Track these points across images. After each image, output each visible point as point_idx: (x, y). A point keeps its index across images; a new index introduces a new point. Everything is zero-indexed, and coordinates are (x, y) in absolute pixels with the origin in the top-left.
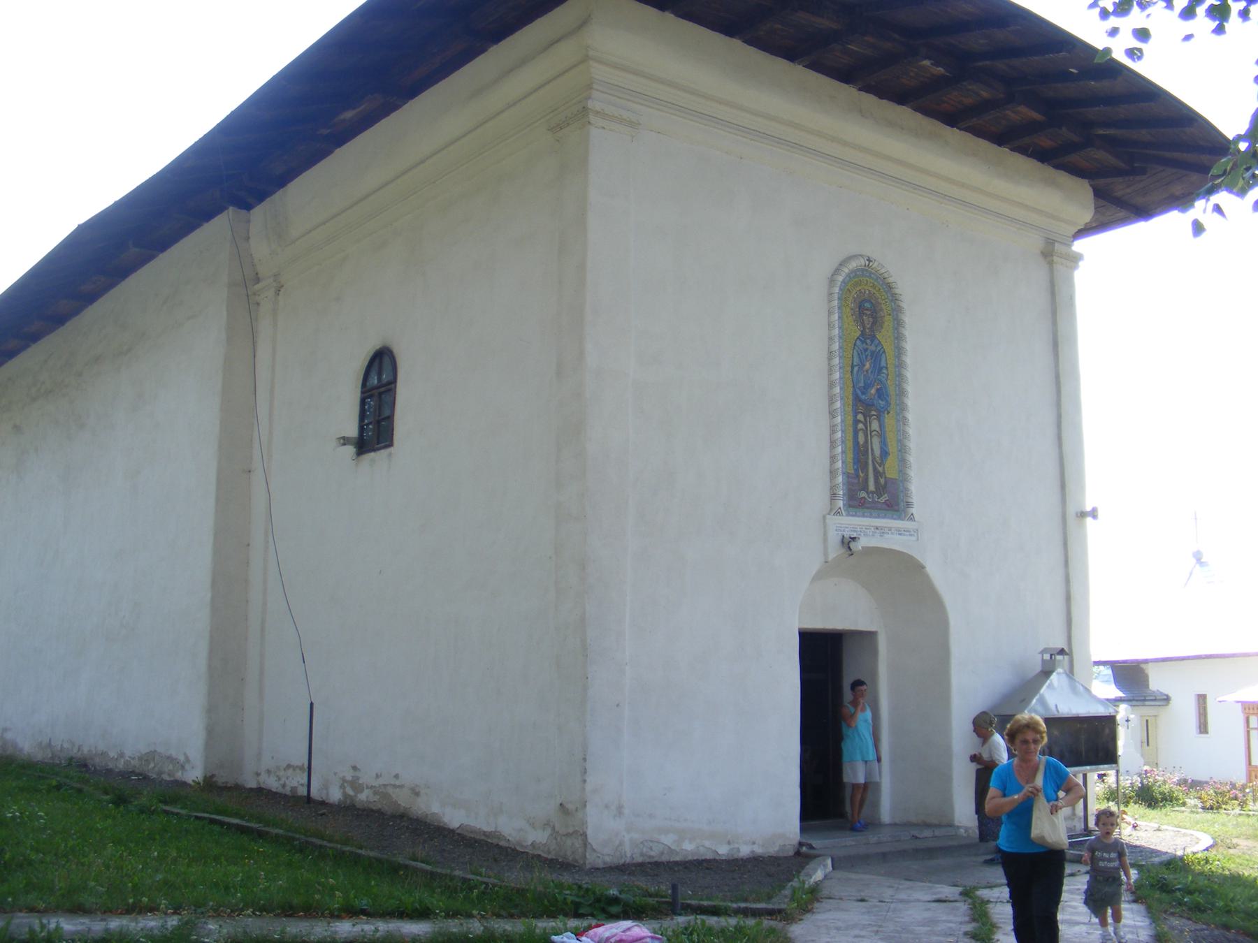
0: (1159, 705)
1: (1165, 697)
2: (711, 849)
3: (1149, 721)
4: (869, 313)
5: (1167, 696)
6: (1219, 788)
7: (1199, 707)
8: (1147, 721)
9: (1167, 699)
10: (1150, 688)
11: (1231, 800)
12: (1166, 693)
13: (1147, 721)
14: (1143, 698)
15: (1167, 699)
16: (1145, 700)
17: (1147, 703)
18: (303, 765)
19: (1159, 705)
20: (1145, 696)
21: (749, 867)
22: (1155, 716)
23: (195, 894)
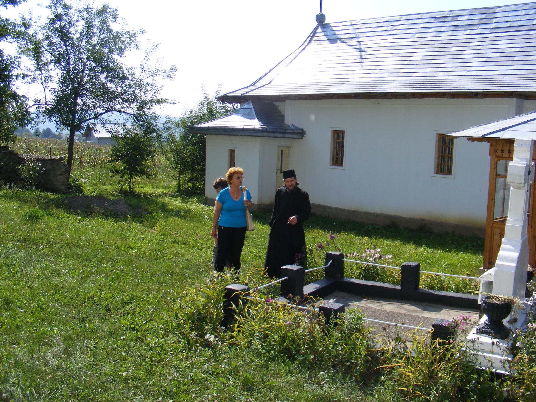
0: (293, 138)
1: (301, 132)
2: (143, 225)
3: (283, 151)
4: (89, 93)
5: (302, 130)
6: (183, 255)
7: (334, 141)
8: (282, 151)
9: (301, 133)
10: (285, 123)
11: (510, 377)
12: (301, 127)
13: (282, 151)
14: (284, 131)
15: (301, 133)
16: (285, 133)
17: (287, 136)
18: (14, 140)
19: (293, 138)
20: (286, 130)
21: (522, 391)
22: (288, 147)
23: (161, 160)
